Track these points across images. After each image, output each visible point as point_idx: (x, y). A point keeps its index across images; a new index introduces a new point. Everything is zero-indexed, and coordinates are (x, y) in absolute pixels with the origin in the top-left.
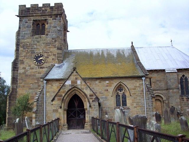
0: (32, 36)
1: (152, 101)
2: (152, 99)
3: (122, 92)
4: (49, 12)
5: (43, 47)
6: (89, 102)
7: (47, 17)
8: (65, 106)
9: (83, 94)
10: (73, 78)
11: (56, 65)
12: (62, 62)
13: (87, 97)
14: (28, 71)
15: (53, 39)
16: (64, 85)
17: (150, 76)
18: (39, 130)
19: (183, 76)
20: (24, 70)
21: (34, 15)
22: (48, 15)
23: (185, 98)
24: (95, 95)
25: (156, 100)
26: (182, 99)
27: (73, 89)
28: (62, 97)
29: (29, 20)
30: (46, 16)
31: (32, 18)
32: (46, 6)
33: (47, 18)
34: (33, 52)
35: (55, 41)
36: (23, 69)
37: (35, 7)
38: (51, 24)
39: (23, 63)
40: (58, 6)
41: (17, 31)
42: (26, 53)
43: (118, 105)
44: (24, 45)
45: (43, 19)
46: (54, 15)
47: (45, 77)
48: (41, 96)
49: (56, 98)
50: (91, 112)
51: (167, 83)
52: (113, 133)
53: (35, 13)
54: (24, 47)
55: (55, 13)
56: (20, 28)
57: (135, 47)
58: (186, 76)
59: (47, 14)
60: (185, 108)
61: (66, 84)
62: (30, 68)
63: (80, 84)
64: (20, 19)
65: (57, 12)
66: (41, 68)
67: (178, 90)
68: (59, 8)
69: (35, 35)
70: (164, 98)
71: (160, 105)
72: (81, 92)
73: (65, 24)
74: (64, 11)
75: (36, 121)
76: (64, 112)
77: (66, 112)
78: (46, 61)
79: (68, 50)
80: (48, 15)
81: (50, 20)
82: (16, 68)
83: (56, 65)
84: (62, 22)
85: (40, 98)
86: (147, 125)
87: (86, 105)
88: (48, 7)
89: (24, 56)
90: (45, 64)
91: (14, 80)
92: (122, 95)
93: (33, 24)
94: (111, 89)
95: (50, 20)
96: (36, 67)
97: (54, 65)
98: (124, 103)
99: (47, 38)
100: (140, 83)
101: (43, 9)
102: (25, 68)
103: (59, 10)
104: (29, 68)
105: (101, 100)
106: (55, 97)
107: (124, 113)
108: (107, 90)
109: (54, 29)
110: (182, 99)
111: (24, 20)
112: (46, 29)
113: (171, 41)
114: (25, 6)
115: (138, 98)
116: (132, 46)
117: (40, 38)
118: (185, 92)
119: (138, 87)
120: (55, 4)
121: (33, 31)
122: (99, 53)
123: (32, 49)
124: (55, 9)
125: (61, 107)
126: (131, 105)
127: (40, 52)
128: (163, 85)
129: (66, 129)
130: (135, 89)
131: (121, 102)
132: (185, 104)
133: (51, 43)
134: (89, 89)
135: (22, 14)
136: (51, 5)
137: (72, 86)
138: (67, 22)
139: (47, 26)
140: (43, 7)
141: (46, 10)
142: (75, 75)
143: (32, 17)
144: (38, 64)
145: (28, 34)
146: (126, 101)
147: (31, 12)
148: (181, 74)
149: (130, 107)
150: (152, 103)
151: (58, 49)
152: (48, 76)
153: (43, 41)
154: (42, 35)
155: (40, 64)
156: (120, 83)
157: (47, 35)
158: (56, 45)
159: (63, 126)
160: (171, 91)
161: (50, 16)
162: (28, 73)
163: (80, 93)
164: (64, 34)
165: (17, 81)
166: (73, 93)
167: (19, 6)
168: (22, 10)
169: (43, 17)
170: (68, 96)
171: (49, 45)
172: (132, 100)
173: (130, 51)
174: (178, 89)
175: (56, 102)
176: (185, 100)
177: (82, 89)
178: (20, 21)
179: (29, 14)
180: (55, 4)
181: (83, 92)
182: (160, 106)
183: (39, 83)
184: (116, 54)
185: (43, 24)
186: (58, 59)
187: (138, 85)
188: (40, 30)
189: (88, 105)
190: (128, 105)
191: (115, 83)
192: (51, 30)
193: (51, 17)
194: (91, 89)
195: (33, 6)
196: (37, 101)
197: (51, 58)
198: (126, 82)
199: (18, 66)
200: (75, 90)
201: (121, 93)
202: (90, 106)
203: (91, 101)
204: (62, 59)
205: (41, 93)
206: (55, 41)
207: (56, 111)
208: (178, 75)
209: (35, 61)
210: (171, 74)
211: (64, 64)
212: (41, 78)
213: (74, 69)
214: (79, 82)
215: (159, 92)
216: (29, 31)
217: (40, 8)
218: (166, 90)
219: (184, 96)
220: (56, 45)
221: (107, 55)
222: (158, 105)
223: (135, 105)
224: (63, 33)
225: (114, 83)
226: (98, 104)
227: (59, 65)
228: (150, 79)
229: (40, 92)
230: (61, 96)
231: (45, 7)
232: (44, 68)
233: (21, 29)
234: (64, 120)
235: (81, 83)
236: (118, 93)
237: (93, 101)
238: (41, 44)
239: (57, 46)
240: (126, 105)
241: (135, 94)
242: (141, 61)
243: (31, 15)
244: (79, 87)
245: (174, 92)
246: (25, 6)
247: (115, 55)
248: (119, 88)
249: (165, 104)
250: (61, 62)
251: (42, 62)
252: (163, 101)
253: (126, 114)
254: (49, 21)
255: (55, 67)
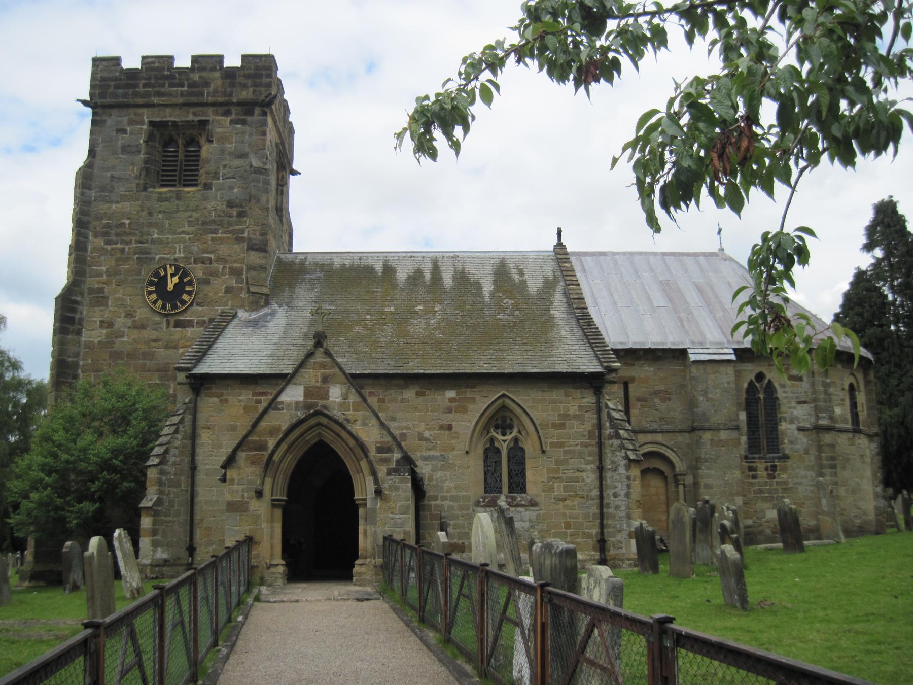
0: (145, 189)
1: (628, 478)
2: (628, 468)
3: (508, 437)
4: (216, 92)
5: (187, 237)
6: (374, 473)
7: (210, 110)
8: (275, 488)
9: (352, 443)
10: (311, 376)
11: (242, 314)
12: (267, 304)
13: (367, 456)
14: (123, 336)
15: (230, 204)
16: (273, 405)
17: (627, 372)
18: (186, 587)
19: (760, 377)
20: (104, 331)
21: (155, 100)
22: (213, 104)
23: (761, 466)
24: (400, 446)
25: (644, 472)
26: (751, 469)
27: (313, 421)
28: (266, 454)
29: (131, 122)
30: (205, 109)
31: (146, 115)
32: (206, 64)
33: (210, 115)
34: (144, 257)
35: (241, 215)
36: (101, 326)
37: (158, 68)
38: (223, 139)
39: (100, 299)
40: (257, 68)
41: (82, 164)
42: (117, 260)
43: (491, 486)
44: (108, 226)
45: (191, 117)
46: (239, 104)
47: (195, 366)
48: (178, 443)
49: (242, 455)
50: (384, 517)
51: (692, 404)
52: (464, 604)
53: (158, 94)
54: (106, 234)
55: (246, 94)
56: (92, 152)
57: (569, 250)
58: (769, 376)
59: (210, 99)
60: (761, 505)
61: (285, 398)
62: (130, 324)
63: (338, 400)
64: (94, 114)
65: (254, 91)
66: (178, 324)
67: (734, 434)
68: (260, 76)
69: (154, 187)
70: (680, 466)
71: (662, 491)
72: (343, 434)
73: (283, 143)
74: (281, 90)
75: (155, 545)
76: (272, 515)
77: (278, 513)
78: (201, 295)
79: (290, 251)
80: (213, 104)
81: (221, 125)
82: (71, 321)
83: (242, 314)
84: (271, 136)
85: (173, 451)
86: (580, 579)
87: (364, 488)
88: (213, 69)
89: (108, 273)
90: (195, 308)
91: (63, 367)
92: (510, 450)
93: (150, 138)
94: (466, 423)
95: (221, 125)
96: (157, 318)
97: (235, 316)
98: (518, 484)
99: (206, 199)
100: (584, 400)
101: (196, 77)
102: (110, 325)
103: (260, 85)
104: (129, 322)
105: (424, 469)
106: (235, 451)
107: (510, 522)
108: (450, 427)
109: (237, 162)
110: (751, 469)
111: (112, 119)
112: (201, 163)
113: (719, 233)
114: (117, 60)
115: (574, 463)
116: (560, 245)
117: (179, 198)
118: (764, 442)
119: (575, 417)
120: (245, 58)
121: (147, 170)
122: (419, 273)
123: (141, 242)
124: (241, 80)
125: (259, 494)
126: (544, 491)
127: (176, 260)
128: (675, 410)
129: (280, 582)
130: (562, 426)
131: (505, 475)
132: (761, 491)
133: (221, 224)
134: (374, 421)
135: (102, 95)
136: (227, 64)
137: (307, 406)
138: (291, 131)
139: (207, 150)
140: (192, 69)
141: (206, 84)
142: (323, 366)
143: (145, 111)
144: (164, 307)
145: (127, 180)
146: (523, 474)
147: (141, 89)
148: (750, 371)
149: (541, 500)
150: (628, 486)
151: (253, 249)
152: (208, 360)
153: (189, 213)
154: (185, 186)
155: (174, 307)
156: (500, 401)
157: (207, 187)
158: (243, 231)
159: (268, 568)
160: (707, 436)
161: (221, 110)
162: (125, 342)
163: (338, 435)
164: (278, 185)
165: (75, 377)
166: (311, 438)
167: (95, 60)
168: (103, 79)
169: (191, 110)
170: (289, 447)
171: (215, 232)
172: (549, 470)
173: (549, 269)
174: (737, 428)
175: (247, 472)
176: (762, 473)
177: (348, 421)
178: (94, 123)
179: (136, 95)
180: (245, 58)
181: (350, 433)
182: (663, 498)
183: (168, 387)
184: (490, 278)
185: (192, 141)
186: (249, 291)
187: (573, 409)
188: (178, 169)
189: (371, 486)
190: (532, 489)
191: (483, 401)
192: (225, 166)
193: (227, 113)
194: (382, 425)
195: (153, 63)
196: (160, 464)
197: (219, 285)
198: (526, 399)
199: (81, 313)
200: (319, 424)
201: (504, 441)
202: (378, 492)
203: (382, 470)
204: (265, 290)
205: (176, 432)
206: (241, 215)
207: (235, 507)
208: (738, 374)
209: (154, 297)
210: (709, 368)
211: (273, 314)
212: (180, 370)
213: (319, 340)
214: (335, 393)
215: (659, 438)
216: (131, 168)
217: (182, 71)
218: (689, 432)
219: (760, 458)
220: (243, 231)
221: (454, 278)
222: (653, 490)
223: (559, 489)
224: (273, 183)
225: (478, 398)
226: (410, 485)
227: (254, 316)
228: (626, 385)
229: (173, 428)
230: (262, 447)
231: (202, 69)
232: (189, 324)
233: (98, 157)
234: (272, 547)
235: (345, 397)
236: (492, 440)
237: (389, 473)
238: (177, 230)
239: (245, 235)
240: (523, 489)
241: (560, 447)
242: (592, 311)
243: (139, 101)
244: (337, 413)
245: (716, 443)
246: (117, 60)
247: (487, 287)
248: (500, 419)
249: (681, 487)
250: (259, 301)
251: (183, 302)
252: (675, 476)
253: (517, 524)
254: (219, 130)
255: (235, 322)
